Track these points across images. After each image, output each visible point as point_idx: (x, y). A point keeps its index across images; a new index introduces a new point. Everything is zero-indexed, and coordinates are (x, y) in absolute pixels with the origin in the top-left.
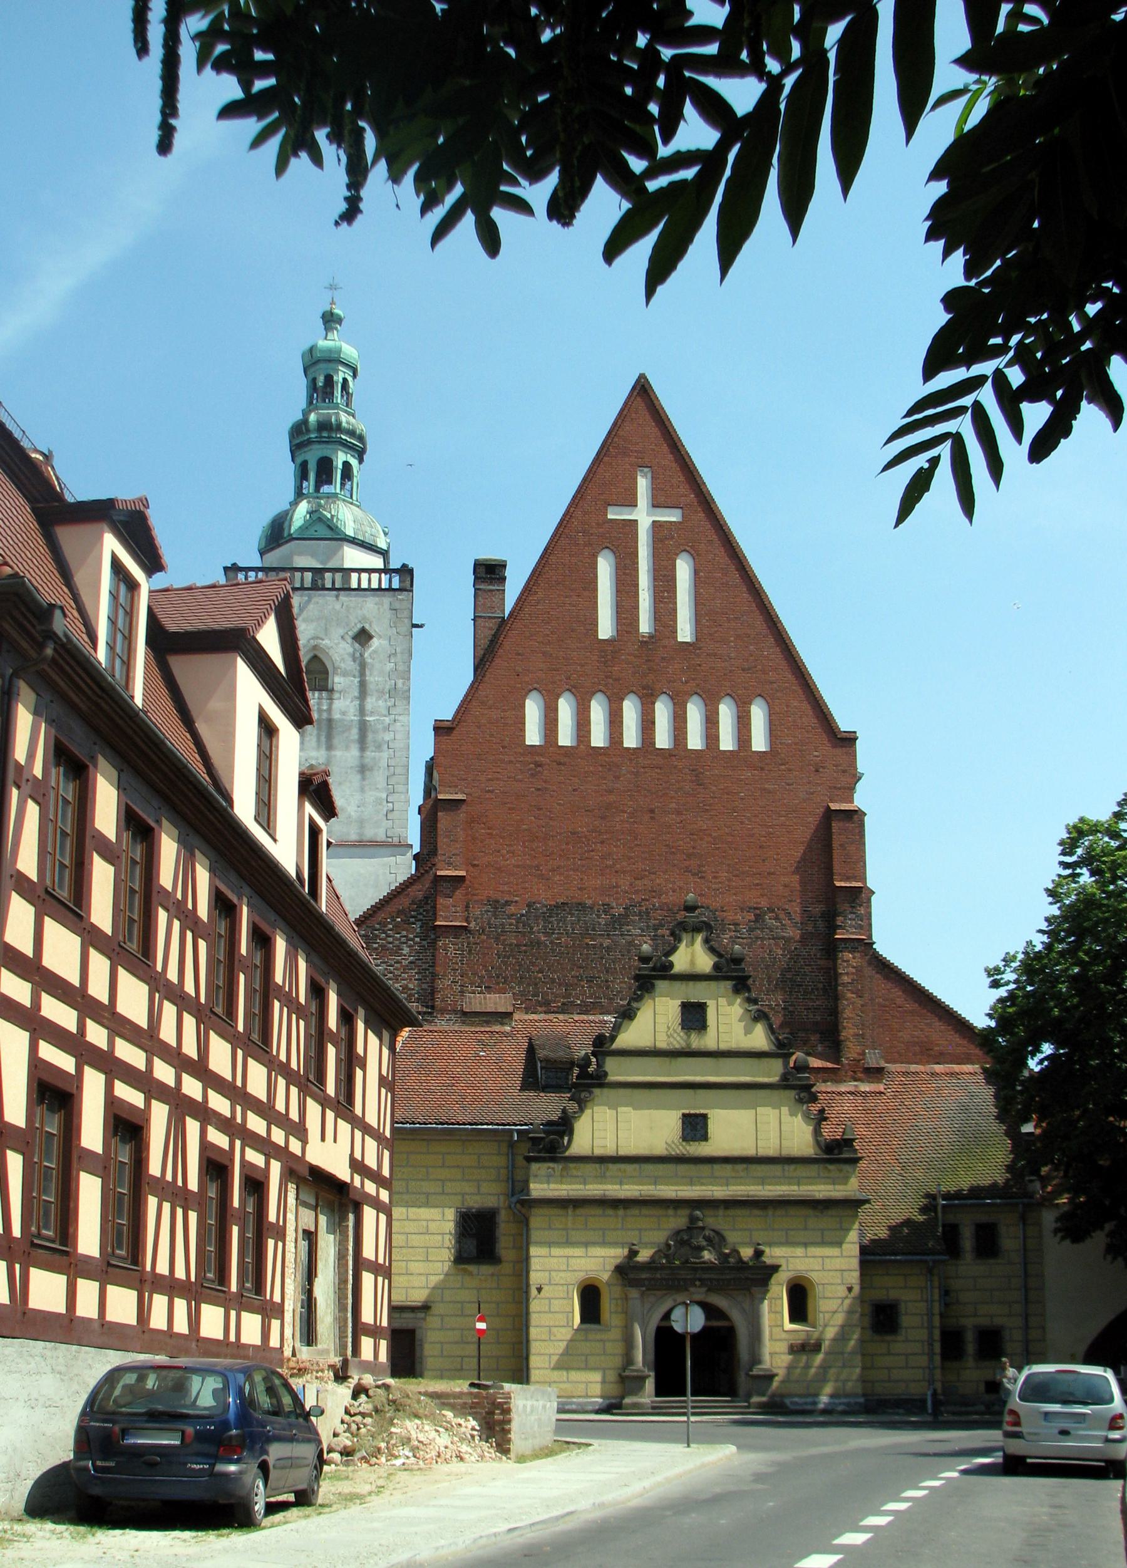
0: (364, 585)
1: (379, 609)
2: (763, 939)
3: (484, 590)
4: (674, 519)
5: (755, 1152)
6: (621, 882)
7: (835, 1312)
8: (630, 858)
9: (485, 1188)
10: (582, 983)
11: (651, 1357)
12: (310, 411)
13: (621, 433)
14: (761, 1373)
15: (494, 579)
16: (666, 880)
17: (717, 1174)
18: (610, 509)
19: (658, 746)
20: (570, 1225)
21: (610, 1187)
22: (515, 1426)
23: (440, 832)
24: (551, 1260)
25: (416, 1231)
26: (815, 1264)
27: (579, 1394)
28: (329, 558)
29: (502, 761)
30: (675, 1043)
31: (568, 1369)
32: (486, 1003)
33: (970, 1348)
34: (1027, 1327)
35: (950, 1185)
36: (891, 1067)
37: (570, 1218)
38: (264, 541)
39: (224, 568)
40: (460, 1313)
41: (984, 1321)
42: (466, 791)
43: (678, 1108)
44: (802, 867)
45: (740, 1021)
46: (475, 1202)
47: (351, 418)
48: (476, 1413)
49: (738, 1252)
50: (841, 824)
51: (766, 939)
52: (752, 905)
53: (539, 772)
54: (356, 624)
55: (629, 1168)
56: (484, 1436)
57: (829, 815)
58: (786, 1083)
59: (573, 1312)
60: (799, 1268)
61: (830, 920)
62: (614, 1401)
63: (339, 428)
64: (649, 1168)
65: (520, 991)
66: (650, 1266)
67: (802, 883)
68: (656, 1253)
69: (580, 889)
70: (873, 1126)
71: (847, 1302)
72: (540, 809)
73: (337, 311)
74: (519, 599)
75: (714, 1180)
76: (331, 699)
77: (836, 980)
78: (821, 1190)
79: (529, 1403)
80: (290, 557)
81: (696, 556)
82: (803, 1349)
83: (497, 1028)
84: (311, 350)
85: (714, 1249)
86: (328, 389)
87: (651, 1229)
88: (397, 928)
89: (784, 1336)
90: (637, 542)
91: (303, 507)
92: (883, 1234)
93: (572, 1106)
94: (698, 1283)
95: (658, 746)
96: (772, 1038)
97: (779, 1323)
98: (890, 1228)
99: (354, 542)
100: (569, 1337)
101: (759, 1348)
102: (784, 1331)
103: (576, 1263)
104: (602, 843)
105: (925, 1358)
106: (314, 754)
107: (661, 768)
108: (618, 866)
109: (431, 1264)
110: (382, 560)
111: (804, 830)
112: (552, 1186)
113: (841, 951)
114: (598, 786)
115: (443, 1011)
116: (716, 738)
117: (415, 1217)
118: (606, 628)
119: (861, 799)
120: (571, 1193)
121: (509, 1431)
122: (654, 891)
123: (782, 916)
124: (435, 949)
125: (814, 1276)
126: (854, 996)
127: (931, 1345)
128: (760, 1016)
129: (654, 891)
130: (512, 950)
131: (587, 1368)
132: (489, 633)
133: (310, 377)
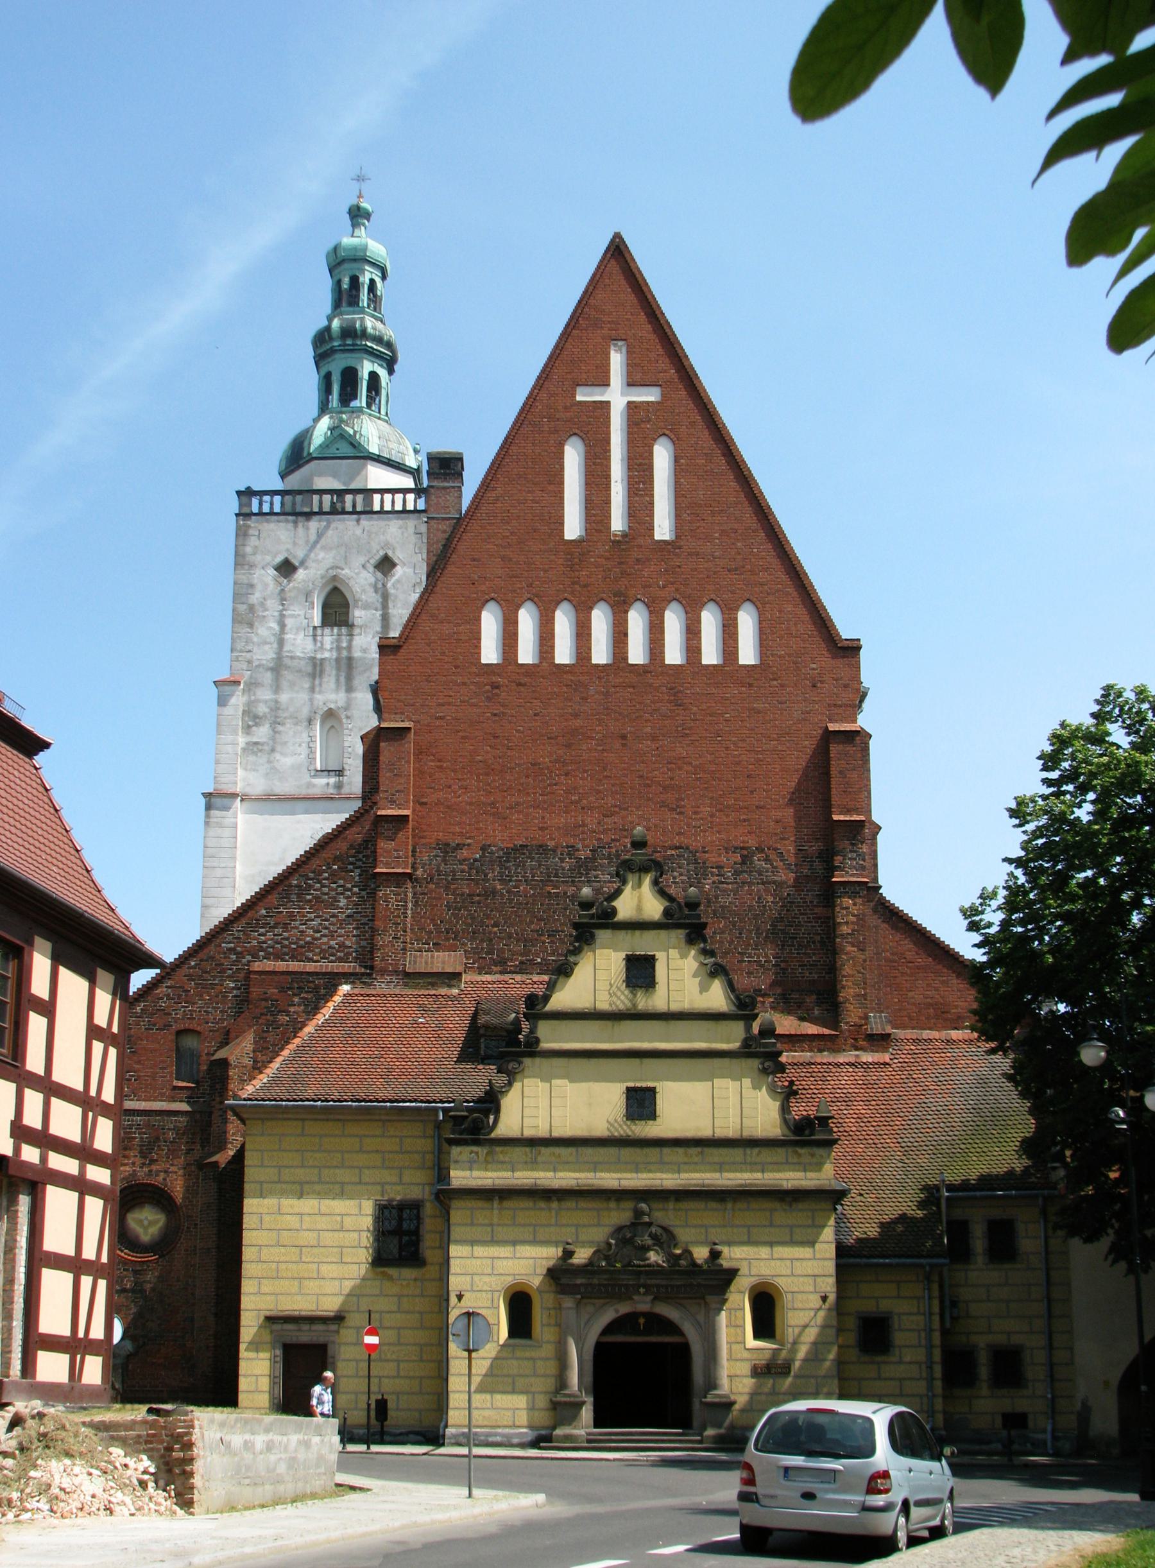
0: (388, 507)
1: (403, 533)
2: (750, 884)
3: (438, 488)
5: (739, 1133)
7: (805, 1326)
8: (599, 792)
9: (410, 1176)
10: (543, 938)
11: (589, 1379)
12: (335, 317)
13: (592, 301)
14: (717, 1400)
15: (448, 474)
16: (639, 817)
17: (666, 1159)
18: (579, 390)
19: (631, 661)
20: (495, 1220)
21: (542, 1174)
22: (199, 1467)
23: (382, 766)
25: (330, 1227)
26: (783, 1268)
27: (505, 1423)
28: (352, 479)
29: (456, 683)
30: (618, 1002)
31: (492, 1392)
32: (432, 963)
33: (984, 1372)
34: (1051, 1347)
35: (954, 1176)
36: (901, 1033)
37: (496, 1212)
38: (284, 463)
39: (237, 492)
41: (1001, 1339)
42: (414, 717)
43: (621, 1081)
44: (796, 798)
45: (695, 976)
46: (397, 1194)
47: (379, 325)
48: (152, 1449)
49: (691, 1253)
50: (841, 747)
51: (754, 884)
52: (736, 844)
53: (497, 695)
54: (378, 551)
55: (564, 1152)
56: (161, 1483)
57: (828, 737)
58: (748, 1050)
59: (498, 1324)
60: (763, 1272)
61: (828, 859)
62: (543, 1432)
63: (364, 334)
64: (589, 1151)
65: (472, 948)
66: (588, 1269)
67: (798, 818)
68: (595, 1253)
69: (542, 829)
70: (873, 1103)
71: (822, 1314)
72: (496, 737)
73: (365, 205)
74: (476, 496)
75: (662, 1166)
76: (351, 635)
77: (834, 931)
78: (791, 1178)
79: (260, 1440)
80: (310, 479)
81: (676, 441)
83: (443, 991)
84: (336, 249)
85: (662, 1249)
87: (590, 1226)
88: (333, 877)
89: (746, 1355)
90: (609, 427)
91: (325, 422)
92: (873, 1231)
93: (500, 1080)
94: (642, 1290)
95: (631, 661)
97: (740, 1339)
98: (882, 1225)
99: (378, 460)
101: (715, 1369)
104: (566, 774)
105: (924, 1383)
106: (333, 697)
107: (634, 687)
108: (585, 801)
109: (346, 1267)
110: (412, 480)
111: (799, 757)
112: (476, 1173)
113: (840, 897)
114: (563, 709)
115: (383, 972)
116: (698, 651)
117: (328, 1211)
118: (573, 527)
120: (497, 1182)
122: (626, 830)
125: (782, 1283)
127: (930, 1368)
128: (717, 971)
129: (626, 830)
131: (513, 1392)
132: (442, 537)
133: (336, 279)
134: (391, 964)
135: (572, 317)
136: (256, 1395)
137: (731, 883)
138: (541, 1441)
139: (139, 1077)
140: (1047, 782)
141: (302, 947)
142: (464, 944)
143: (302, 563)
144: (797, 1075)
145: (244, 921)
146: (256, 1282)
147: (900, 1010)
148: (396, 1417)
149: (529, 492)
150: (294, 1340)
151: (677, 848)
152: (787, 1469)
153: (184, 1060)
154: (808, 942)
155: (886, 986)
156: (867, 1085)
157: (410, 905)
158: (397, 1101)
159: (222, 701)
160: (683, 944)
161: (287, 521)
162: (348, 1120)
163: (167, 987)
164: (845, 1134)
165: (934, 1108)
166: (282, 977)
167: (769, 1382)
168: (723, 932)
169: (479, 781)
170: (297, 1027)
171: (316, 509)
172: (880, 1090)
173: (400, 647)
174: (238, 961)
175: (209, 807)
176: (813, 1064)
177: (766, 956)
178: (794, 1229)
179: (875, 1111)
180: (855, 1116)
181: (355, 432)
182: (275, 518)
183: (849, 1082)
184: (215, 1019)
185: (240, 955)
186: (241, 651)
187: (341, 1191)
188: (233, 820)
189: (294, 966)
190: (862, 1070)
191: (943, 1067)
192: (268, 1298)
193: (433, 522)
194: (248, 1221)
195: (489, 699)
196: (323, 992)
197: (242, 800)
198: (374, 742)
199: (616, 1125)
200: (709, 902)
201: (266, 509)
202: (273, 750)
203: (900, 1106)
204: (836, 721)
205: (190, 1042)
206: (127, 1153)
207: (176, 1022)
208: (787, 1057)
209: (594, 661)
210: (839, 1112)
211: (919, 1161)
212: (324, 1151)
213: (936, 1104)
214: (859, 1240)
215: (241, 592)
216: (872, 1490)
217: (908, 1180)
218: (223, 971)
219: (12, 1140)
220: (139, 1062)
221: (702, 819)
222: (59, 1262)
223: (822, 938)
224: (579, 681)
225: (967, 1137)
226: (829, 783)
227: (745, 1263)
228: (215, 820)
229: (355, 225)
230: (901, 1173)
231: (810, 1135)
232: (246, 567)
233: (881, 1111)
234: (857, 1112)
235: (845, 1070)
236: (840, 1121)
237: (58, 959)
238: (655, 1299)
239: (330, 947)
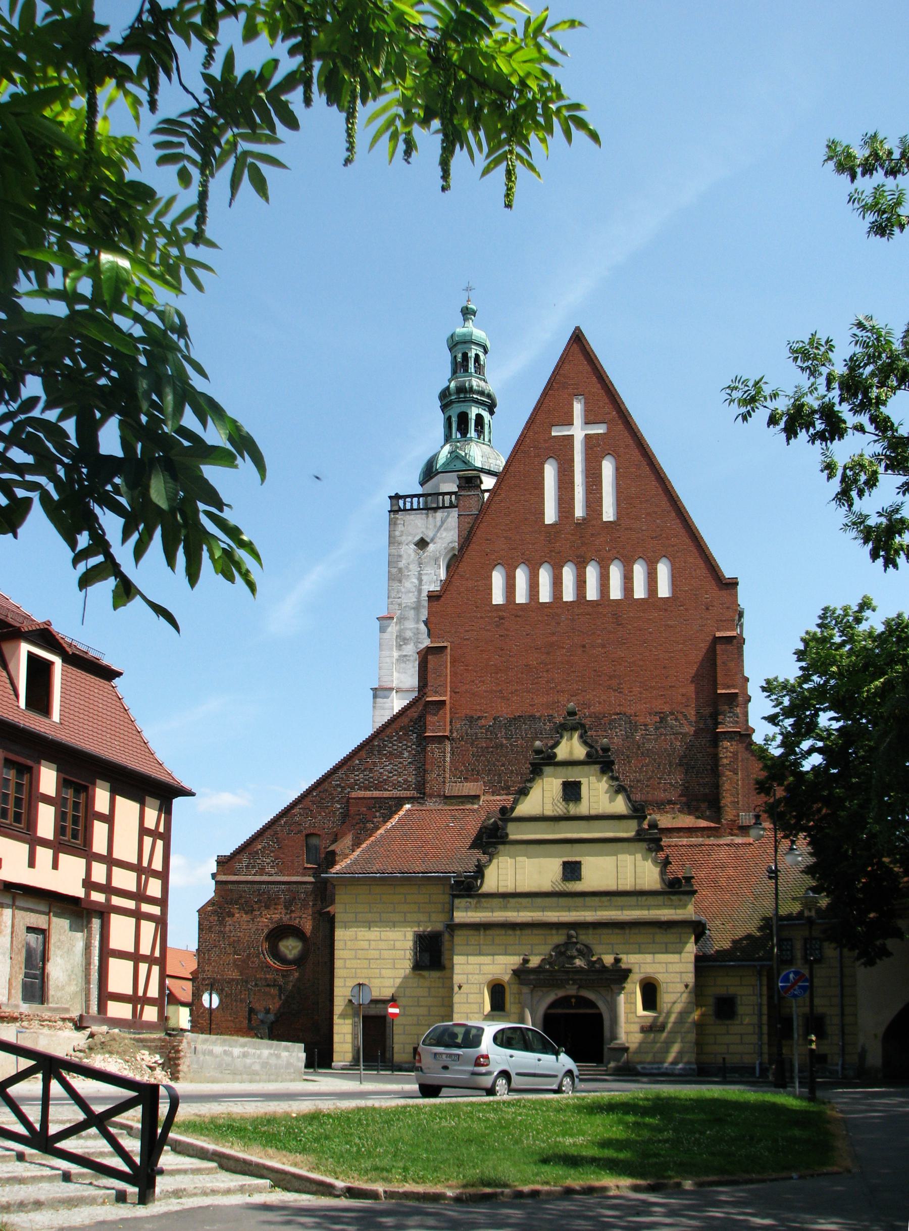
2: (665, 735)
3: (464, 496)
4: (601, 431)
6: (561, 699)
7: (674, 1003)
9: (434, 917)
13: (561, 372)
16: (595, 695)
18: (553, 428)
20: (482, 942)
26: (660, 968)
29: (476, 617)
34: (843, 1014)
44: (696, 679)
47: (482, 384)
57: (717, 640)
58: (639, 837)
60: (648, 970)
63: (471, 390)
64: (539, 901)
66: (538, 970)
71: (685, 995)
73: (471, 306)
75: (586, 908)
78: (666, 914)
79: (237, 1051)
80: (438, 486)
82: (650, 1029)
83: (469, 806)
88: (400, 739)
89: (637, 1020)
90: (573, 451)
91: (447, 448)
92: (727, 945)
93: (484, 858)
97: (633, 1010)
103: (486, 969)
104: (547, 671)
109: (397, 971)
111: (698, 654)
115: (431, 796)
118: (550, 515)
121: (178, 1065)
125: (660, 977)
127: (760, 1027)
128: (619, 790)
135: (548, 383)
140: (801, 668)
143: (432, 540)
145: (345, 768)
151: (618, 714)
152: (435, 1054)
156: (737, 858)
158: (426, 873)
159: (383, 630)
168: (647, 765)
169: (491, 677)
173: (441, 596)
175: (375, 697)
185: (343, 788)
187: (394, 924)
189: (376, 794)
193: (461, 518)
194: (338, 945)
195: (497, 626)
197: (397, 692)
198: (425, 658)
200: (639, 747)
201: (415, 506)
205: (314, 841)
209: (564, 600)
214: (717, 951)
215: (393, 560)
216: (478, 1064)
218: (333, 798)
219: (213, 894)
220: (283, 853)
222: (121, 955)
227: (637, 966)
229: (465, 320)
237: (114, 792)
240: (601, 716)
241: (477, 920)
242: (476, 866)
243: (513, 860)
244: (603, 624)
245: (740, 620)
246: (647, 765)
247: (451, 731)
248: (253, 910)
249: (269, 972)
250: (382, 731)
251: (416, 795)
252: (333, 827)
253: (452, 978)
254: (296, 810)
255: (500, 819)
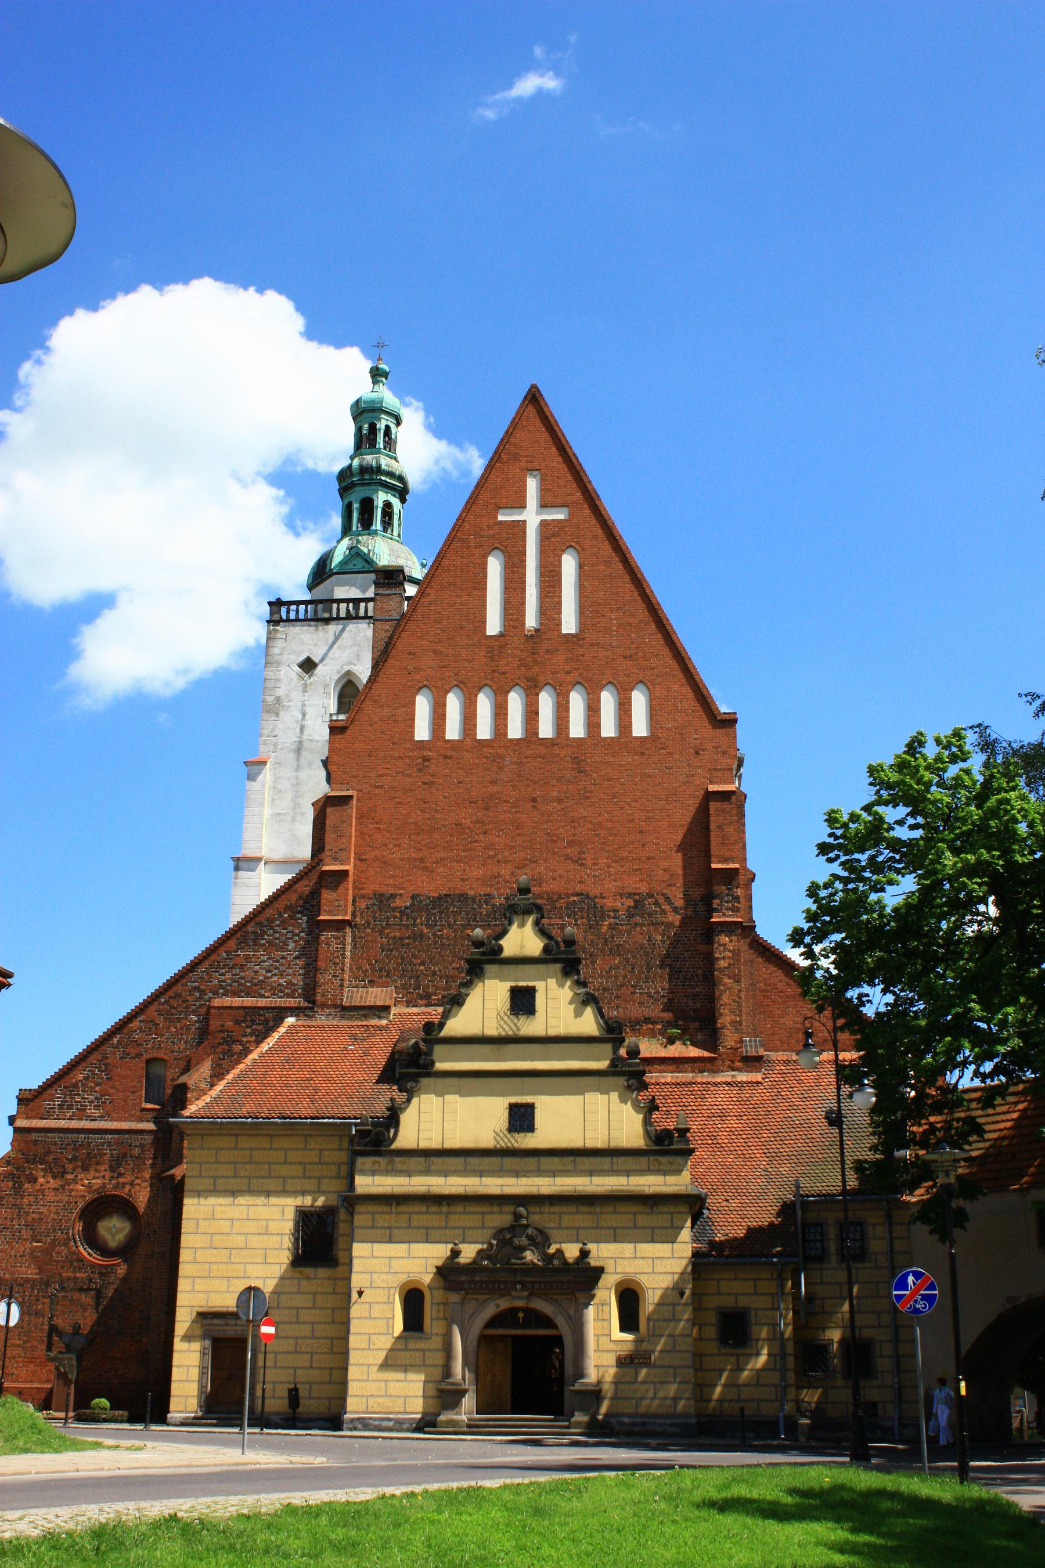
3: (382, 595)
6: (503, 872)
8: (513, 847)
9: (326, 1185)
13: (512, 440)
15: (392, 584)
18: (500, 511)
23: (328, 828)
24: (374, 1260)
25: (256, 1231)
26: (644, 1266)
27: (397, 1410)
29: (393, 758)
30: (507, 1028)
36: (774, 1055)
40: (294, 1319)
42: (357, 787)
44: (683, 847)
45: (570, 1003)
51: (645, 926)
53: (427, 766)
57: (709, 796)
58: (616, 1069)
60: (627, 1270)
63: (379, 470)
65: (401, 984)
66: (472, 1268)
69: (463, 880)
70: (745, 1117)
72: (425, 803)
73: (383, 366)
75: (539, 1172)
82: (627, 1362)
83: (374, 1022)
86: (372, 436)
88: (284, 924)
89: (612, 1346)
93: (400, 1097)
94: (519, 1286)
95: (540, 736)
96: (601, 1021)
97: (606, 1332)
100: (389, 1346)
102: (611, 1341)
103: (398, 1265)
107: (543, 758)
111: (684, 815)
115: (324, 1006)
116: (598, 726)
118: (494, 625)
119: (749, 782)
123: (661, 900)
124: (318, 944)
126: (731, 981)
128: (589, 1000)
130: (395, 944)
132: (385, 635)
133: (358, 426)
134: (330, 999)
136: (186, 1385)
137: (625, 924)
138: (426, 1424)
139: (113, 1100)
141: (256, 985)
142: (396, 981)
144: (679, 1093)
145: (207, 963)
146: (190, 1280)
147: (773, 1034)
148: (307, 1406)
149: (457, 596)
150: (222, 1335)
151: (578, 895)
153: (153, 1086)
154: (692, 975)
155: (760, 1013)
157: (349, 948)
158: (318, 1118)
160: (559, 975)
161: (310, 626)
162: (276, 1135)
163: (140, 1021)
164: (718, 1146)
165: (797, 1122)
166: (237, 1011)
167: (630, 1371)
168: (617, 968)
169: (410, 839)
170: (246, 1052)
171: (335, 616)
172: (751, 1106)
174: (201, 998)
176: (694, 1083)
177: (656, 988)
178: (655, 1230)
179: (745, 1125)
180: (728, 1130)
181: (369, 551)
182: (299, 623)
183: (725, 1099)
184: (179, 1048)
185: (203, 992)
186: (268, 736)
188: (257, 880)
189: (248, 1001)
190: (737, 1088)
191: (808, 1085)
192: (201, 1295)
195: (420, 770)
196: (271, 1024)
197: (266, 863)
198: (324, 808)
199: (501, 1134)
200: (606, 942)
202: (293, 820)
203: (768, 1120)
204: (716, 783)
206: (99, 1167)
207: (146, 1051)
208: (672, 1077)
210: (714, 1126)
211: (781, 1169)
212: (254, 1163)
213: (799, 1118)
217: (769, 1187)
218: (188, 1007)
219: (9, 1148)
221: (600, 869)
223: (704, 971)
224: (497, 753)
225: (825, 1148)
226: (708, 836)
227: (611, 1262)
228: (242, 880)
230: (764, 1180)
231: (669, 1145)
232: (275, 665)
233: (750, 1125)
234: (730, 1126)
235: (722, 1089)
236: (715, 1134)
238: (531, 1294)
239: (279, 985)
240: (555, 897)
241: (387, 1190)
242: (388, 1109)
243: (440, 1099)
244: (560, 770)
245: (738, 770)
246: (617, 968)
247: (354, 914)
248: (65, 1172)
249: (80, 1268)
250: (260, 912)
251: (304, 1004)
252: (186, 1049)
253: (349, 1279)
254: (135, 1024)
255: (424, 1040)
